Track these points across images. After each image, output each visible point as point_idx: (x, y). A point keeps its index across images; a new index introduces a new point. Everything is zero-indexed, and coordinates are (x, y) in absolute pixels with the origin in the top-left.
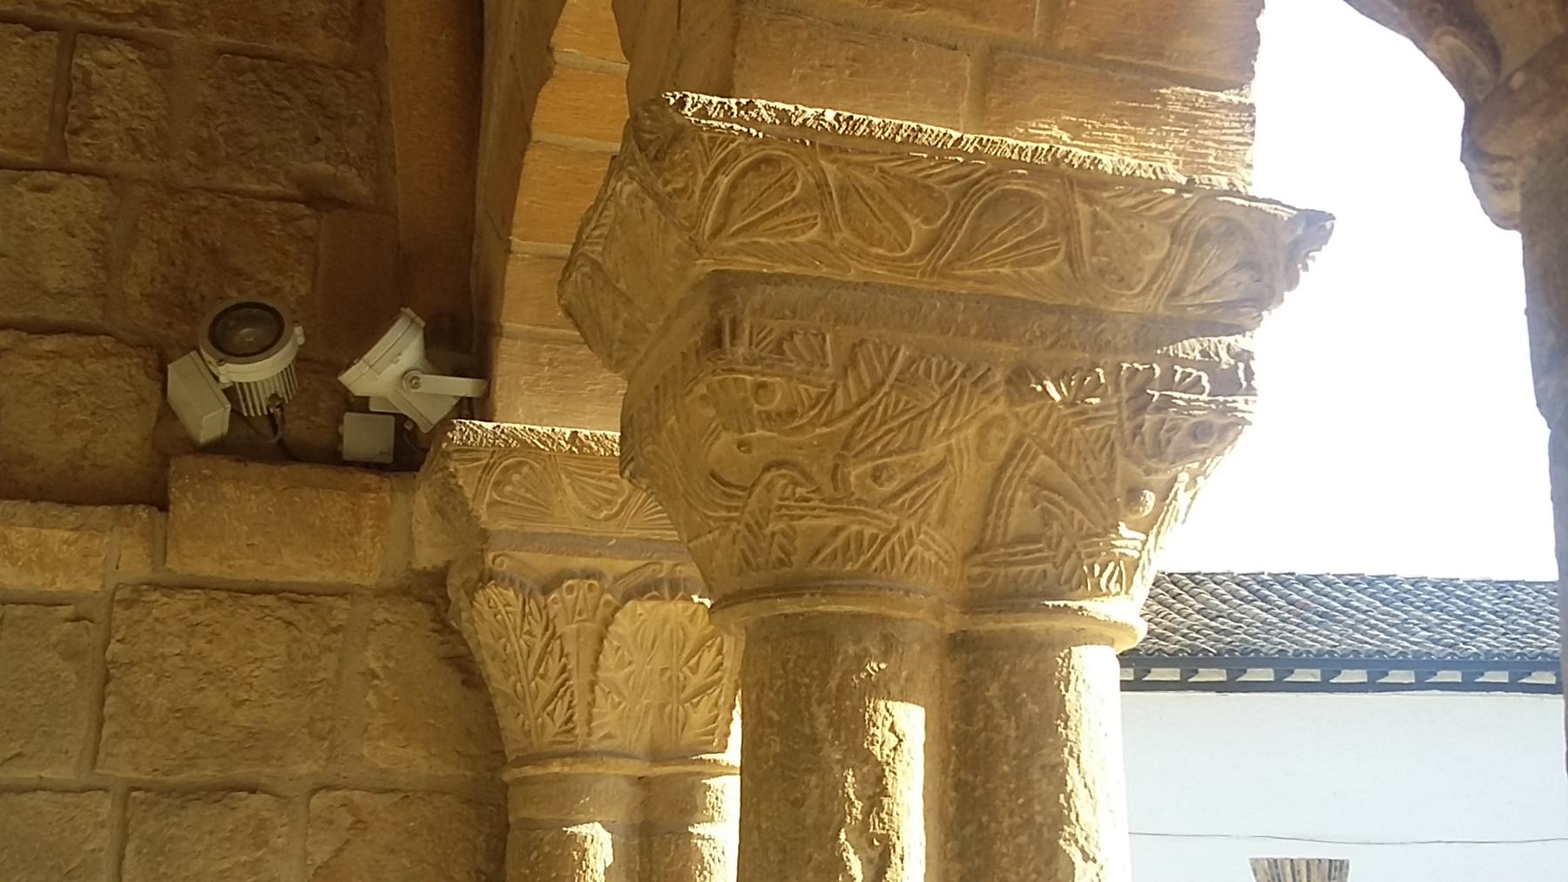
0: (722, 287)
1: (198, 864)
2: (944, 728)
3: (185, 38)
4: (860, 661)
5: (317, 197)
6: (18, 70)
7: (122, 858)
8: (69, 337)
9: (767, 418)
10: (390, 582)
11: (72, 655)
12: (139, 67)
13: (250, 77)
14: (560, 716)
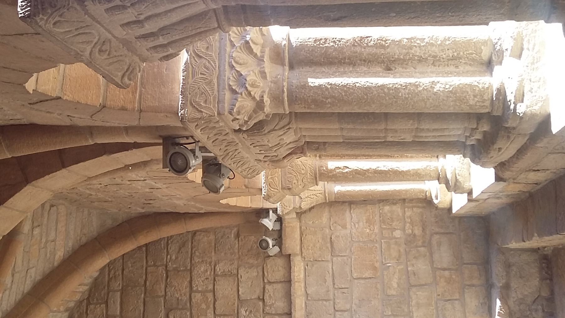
0: (283, 188)
1: (343, 245)
2: (330, 159)
3: (214, 259)
4: (324, 170)
5: (238, 236)
6: (222, 282)
7: (342, 256)
8: (264, 271)
9: (298, 183)
10: (299, 221)
11: (313, 265)
12: (219, 265)
13: (219, 248)
14: (319, 195)
